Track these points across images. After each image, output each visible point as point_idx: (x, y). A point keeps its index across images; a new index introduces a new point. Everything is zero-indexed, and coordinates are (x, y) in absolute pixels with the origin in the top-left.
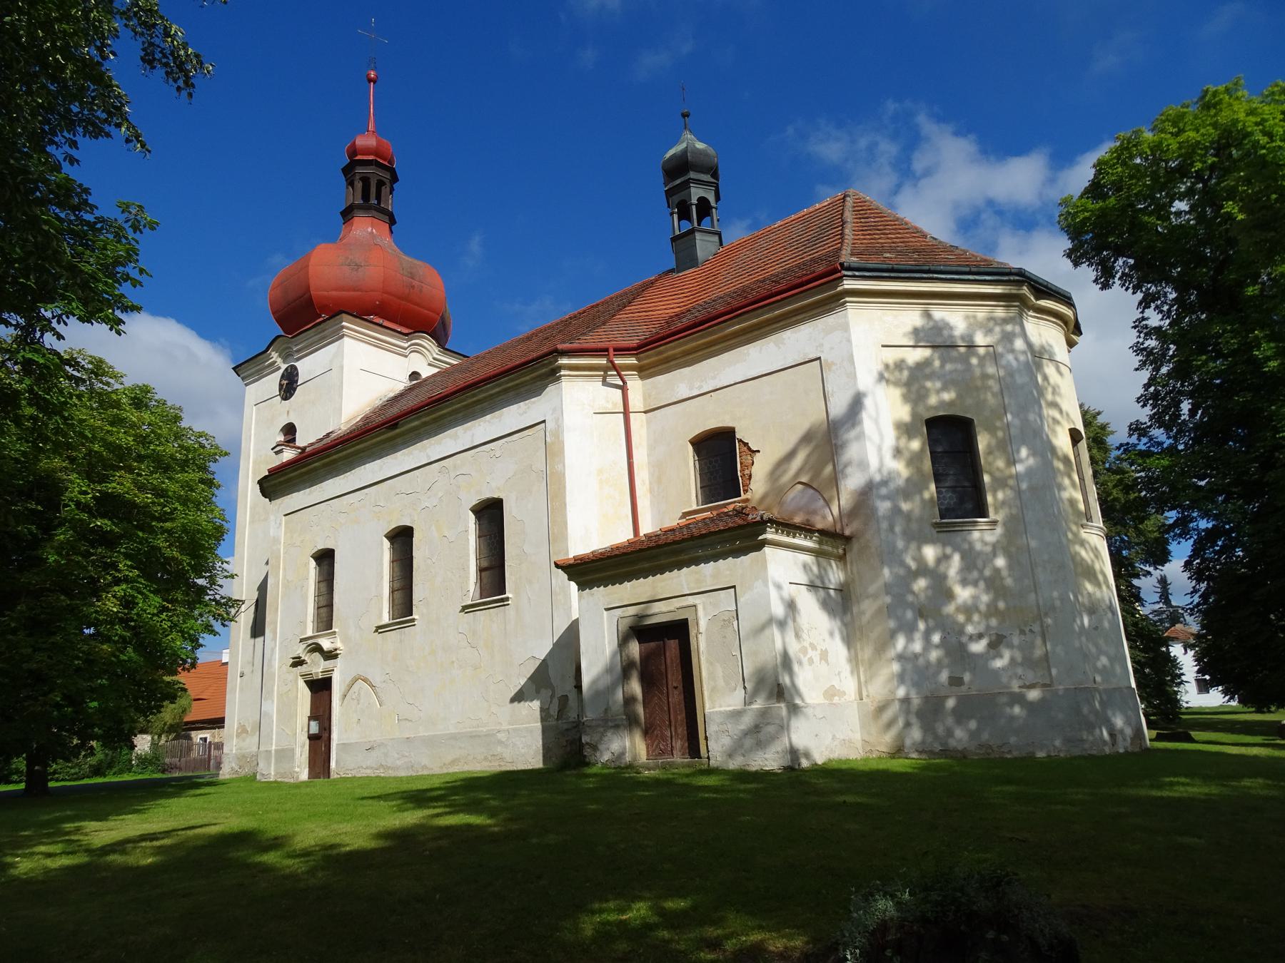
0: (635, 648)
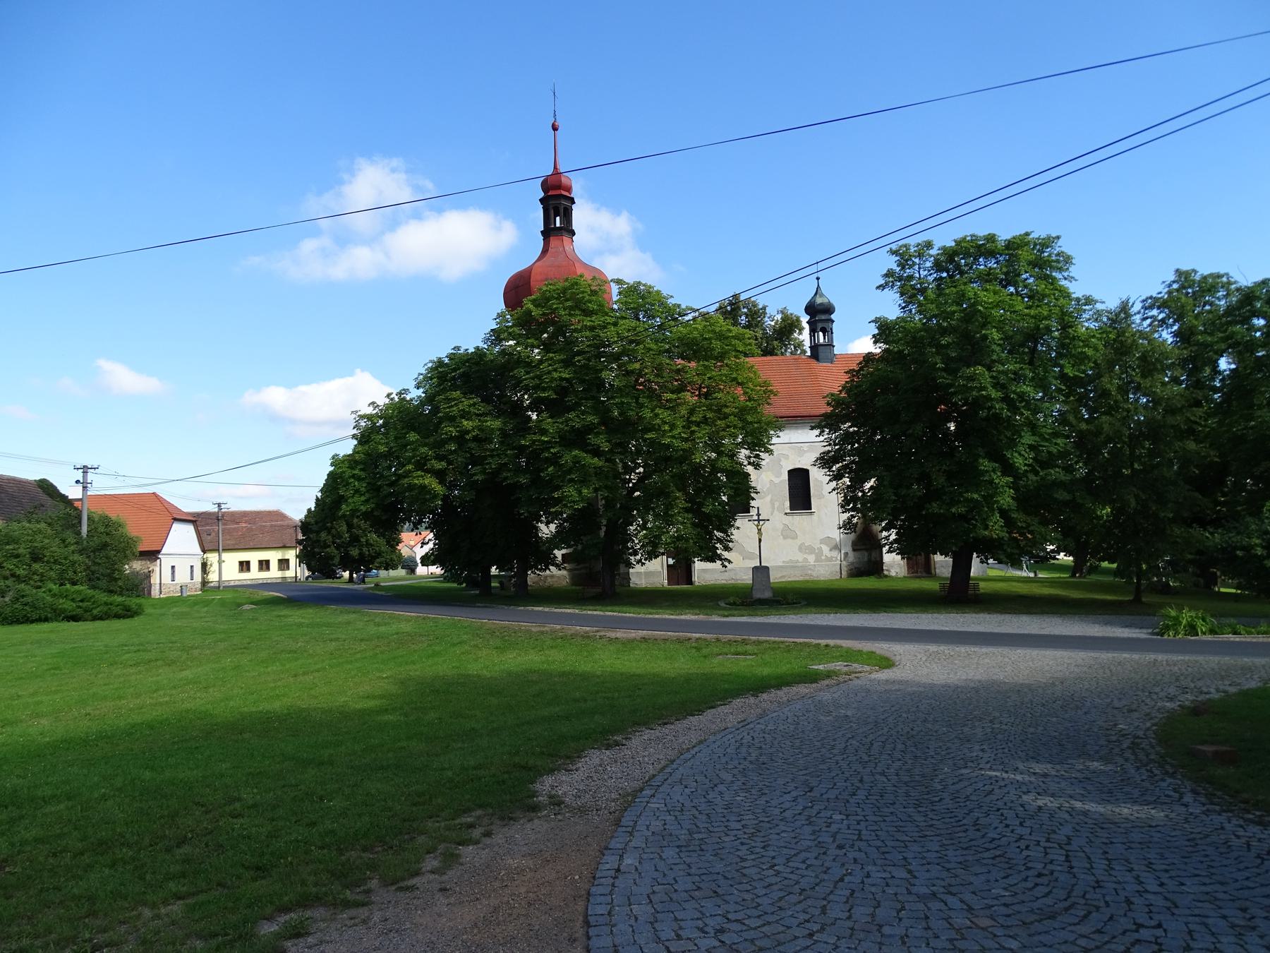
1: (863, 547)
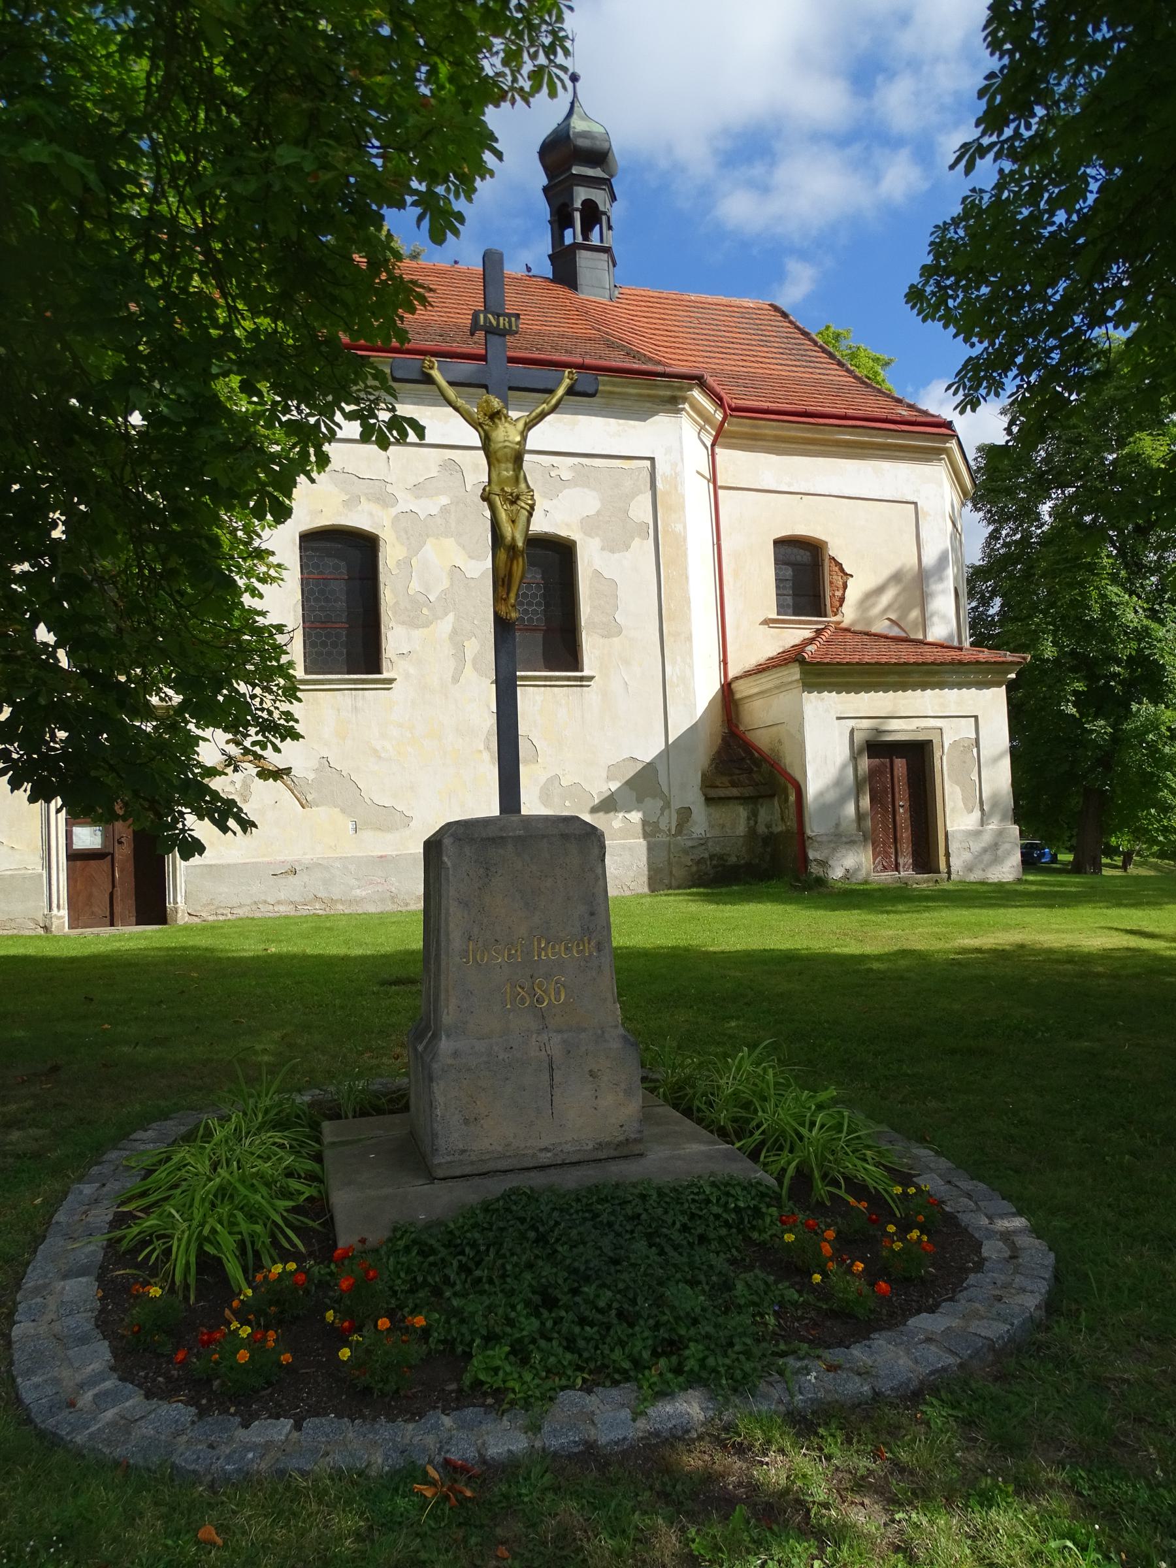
0: (865, 763)
1: (735, 792)
